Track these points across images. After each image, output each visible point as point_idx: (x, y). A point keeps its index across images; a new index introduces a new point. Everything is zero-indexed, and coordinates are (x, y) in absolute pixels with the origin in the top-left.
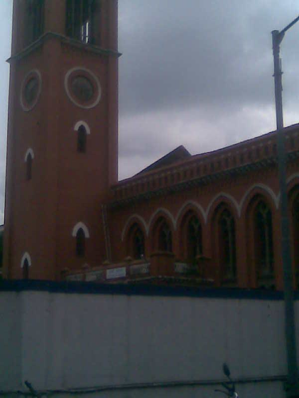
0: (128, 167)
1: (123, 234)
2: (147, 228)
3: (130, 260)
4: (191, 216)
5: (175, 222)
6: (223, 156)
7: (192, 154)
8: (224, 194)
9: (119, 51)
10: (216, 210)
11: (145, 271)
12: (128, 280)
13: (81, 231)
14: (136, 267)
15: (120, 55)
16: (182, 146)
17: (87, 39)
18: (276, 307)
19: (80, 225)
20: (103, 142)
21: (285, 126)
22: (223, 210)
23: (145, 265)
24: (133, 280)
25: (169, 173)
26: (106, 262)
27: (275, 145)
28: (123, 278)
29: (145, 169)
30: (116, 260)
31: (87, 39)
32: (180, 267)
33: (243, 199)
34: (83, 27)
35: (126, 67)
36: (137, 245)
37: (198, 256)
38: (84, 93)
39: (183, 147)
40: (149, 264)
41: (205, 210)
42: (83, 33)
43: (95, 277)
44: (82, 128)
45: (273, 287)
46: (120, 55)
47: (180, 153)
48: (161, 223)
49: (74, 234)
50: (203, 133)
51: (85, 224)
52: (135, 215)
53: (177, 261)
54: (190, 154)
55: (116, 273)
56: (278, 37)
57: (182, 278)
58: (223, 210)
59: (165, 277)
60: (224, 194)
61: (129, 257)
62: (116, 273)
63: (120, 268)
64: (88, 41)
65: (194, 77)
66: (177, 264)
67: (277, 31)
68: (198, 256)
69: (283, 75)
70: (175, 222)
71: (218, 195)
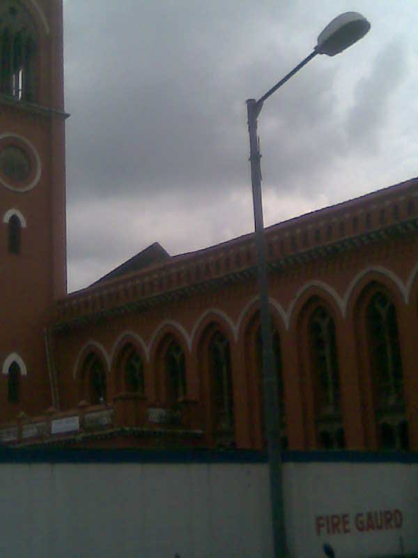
0: (81, 275)
1: (75, 368)
2: (109, 359)
3: (84, 407)
4: (170, 342)
5: (147, 350)
6: (243, 248)
7: (172, 255)
8: (216, 311)
9: (67, 110)
10: (305, 307)
11: (106, 420)
12: (81, 435)
13: (14, 366)
14: (94, 415)
15: (68, 116)
16: (156, 244)
17: (20, 93)
18: (261, 472)
19: (14, 357)
20: (45, 238)
21: (266, 225)
22: (213, 335)
23: (105, 413)
24: (90, 434)
25: (130, 284)
26: (51, 409)
27: (318, 232)
28: (75, 433)
29: (105, 277)
30: (65, 407)
31: (20, 93)
32: (155, 414)
33: (240, 319)
34: (14, 76)
35: (76, 133)
36: (95, 385)
37: (181, 399)
38: (20, 172)
39: (160, 246)
40: (112, 411)
41: (286, 310)
42: (14, 85)
43: (35, 430)
44: (14, 219)
45: (234, 444)
46: (68, 116)
47: (154, 253)
48: (129, 352)
49: (6, 370)
50: (194, 222)
51: (20, 354)
52: (91, 342)
53: (154, 406)
54: (168, 255)
55: (65, 425)
56: (254, 107)
57: (158, 429)
58: (213, 335)
59: (134, 429)
60: (216, 311)
61: (82, 403)
62: (65, 425)
63: (71, 419)
64: (22, 98)
65: (157, 155)
66: (151, 410)
67: (254, 100)
68: (181, 399)
69: (261, 159)
70: (147, 350)
71: (306, 286)
